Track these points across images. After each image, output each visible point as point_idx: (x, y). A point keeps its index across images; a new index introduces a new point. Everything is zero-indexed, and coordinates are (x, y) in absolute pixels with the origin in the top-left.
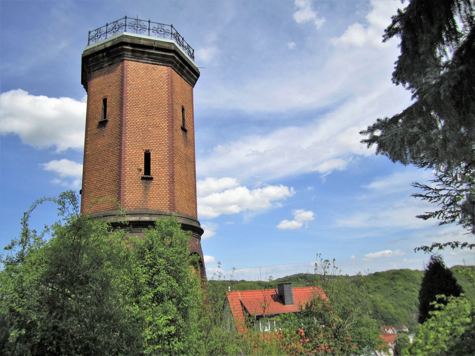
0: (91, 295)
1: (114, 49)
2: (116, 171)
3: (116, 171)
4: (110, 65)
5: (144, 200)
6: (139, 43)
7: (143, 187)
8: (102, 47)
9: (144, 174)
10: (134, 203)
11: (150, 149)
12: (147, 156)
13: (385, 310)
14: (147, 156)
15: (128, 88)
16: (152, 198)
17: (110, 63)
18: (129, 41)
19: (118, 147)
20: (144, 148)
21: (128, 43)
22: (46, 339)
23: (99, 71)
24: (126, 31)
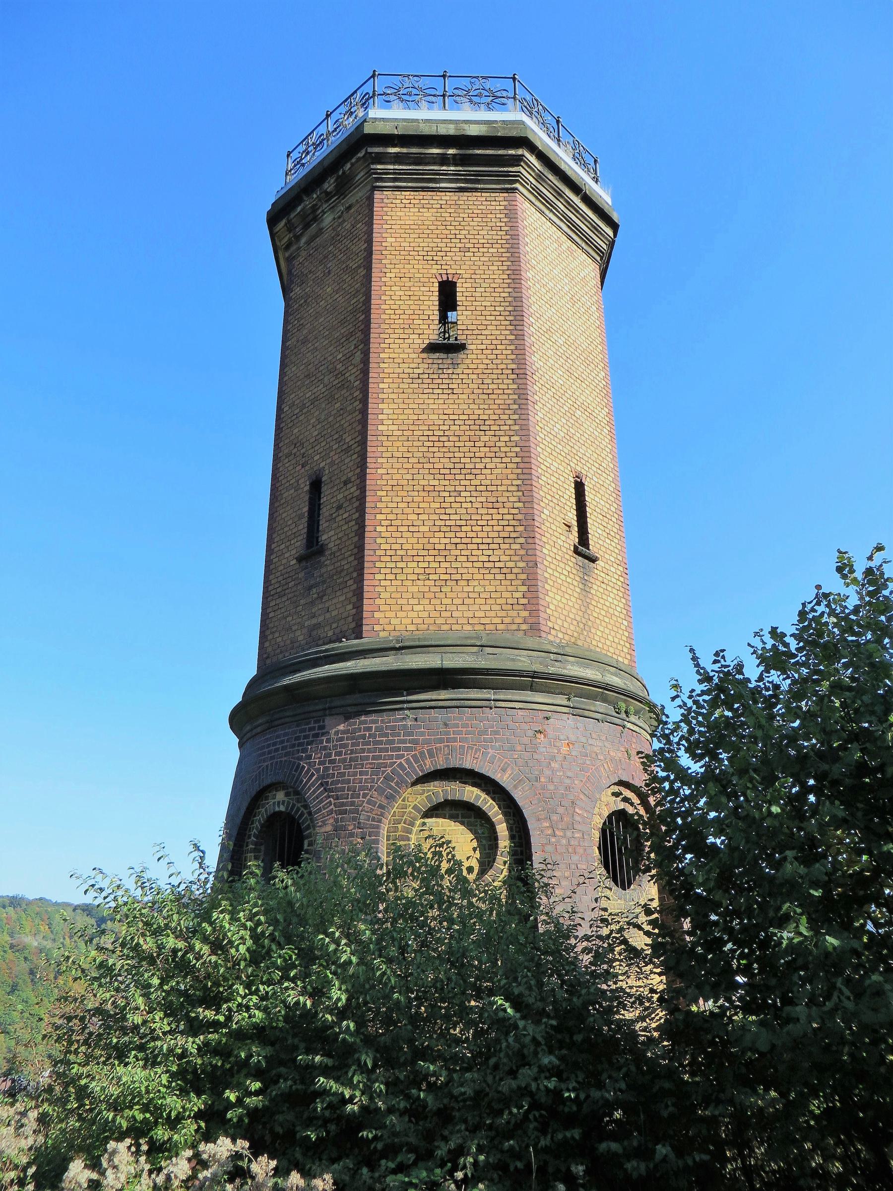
12: (579, 488)
14: (579, 488)
16: (598, 621)
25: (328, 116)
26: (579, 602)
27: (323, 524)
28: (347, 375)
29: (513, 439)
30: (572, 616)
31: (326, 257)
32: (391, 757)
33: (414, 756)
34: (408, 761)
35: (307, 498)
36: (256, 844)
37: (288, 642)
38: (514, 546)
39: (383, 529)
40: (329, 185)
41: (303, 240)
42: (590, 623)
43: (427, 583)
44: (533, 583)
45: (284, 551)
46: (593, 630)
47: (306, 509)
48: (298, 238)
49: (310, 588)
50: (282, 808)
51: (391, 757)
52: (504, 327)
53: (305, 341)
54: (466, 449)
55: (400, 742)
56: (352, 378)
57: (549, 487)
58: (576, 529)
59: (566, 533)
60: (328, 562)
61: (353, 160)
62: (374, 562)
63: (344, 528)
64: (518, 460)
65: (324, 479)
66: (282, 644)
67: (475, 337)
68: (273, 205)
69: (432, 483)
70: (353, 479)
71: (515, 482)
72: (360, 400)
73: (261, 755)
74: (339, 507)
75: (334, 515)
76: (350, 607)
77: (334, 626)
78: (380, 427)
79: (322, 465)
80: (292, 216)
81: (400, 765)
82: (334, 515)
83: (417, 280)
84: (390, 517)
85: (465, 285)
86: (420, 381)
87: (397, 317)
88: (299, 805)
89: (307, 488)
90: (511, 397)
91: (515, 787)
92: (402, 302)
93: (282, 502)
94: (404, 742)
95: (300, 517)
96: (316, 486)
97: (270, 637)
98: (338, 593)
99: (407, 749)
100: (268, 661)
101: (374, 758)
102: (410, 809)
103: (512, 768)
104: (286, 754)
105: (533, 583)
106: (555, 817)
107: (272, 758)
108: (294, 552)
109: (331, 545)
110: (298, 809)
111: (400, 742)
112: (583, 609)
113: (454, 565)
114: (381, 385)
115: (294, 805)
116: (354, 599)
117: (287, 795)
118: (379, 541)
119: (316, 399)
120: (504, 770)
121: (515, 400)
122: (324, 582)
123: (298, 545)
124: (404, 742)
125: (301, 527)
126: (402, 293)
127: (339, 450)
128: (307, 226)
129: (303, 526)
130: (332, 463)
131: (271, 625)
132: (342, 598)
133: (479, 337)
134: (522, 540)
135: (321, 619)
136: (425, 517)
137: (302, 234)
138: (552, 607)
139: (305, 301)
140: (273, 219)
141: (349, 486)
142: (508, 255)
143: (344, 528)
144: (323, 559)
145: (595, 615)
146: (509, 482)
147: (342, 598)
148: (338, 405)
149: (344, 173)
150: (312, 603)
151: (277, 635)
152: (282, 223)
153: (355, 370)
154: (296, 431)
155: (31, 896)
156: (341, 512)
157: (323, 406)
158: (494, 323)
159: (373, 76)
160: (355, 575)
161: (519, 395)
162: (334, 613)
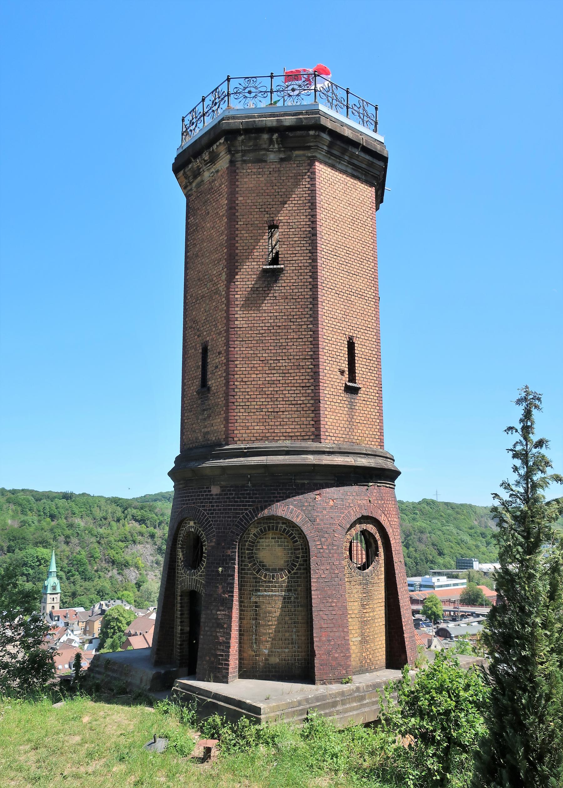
0: (499, 632)
1: (299, 133)
2: (308, 370)
3: (308, 370)
4: (282, 160)
5: (349, 426)
6: (342, 133)
7: (347, 403)
8: (271, 121)
9: (347, 379)
10: (337, 432)
11: (355, 335)
12: (351, 346)
13: (12, 496)
14: (351, 346)
15: (321, 215)
16: (359, 425)
17: (282, 156)
18: (329, 125)
19: (311, 326)
20: (347, 333)
21: (359, 144)
22: (223, 628)
23: (257, 166)
24: (376, 132)
25: (203, 100)
26: (347, 416)
27: (209, 376)
28: (219, 286)
29: (309, 326)
30: (341, 425)
31: (206, 202)
32: (242, 509)
33: (253, 509)
34: (250, 512)
35: (201, 357)
36: (182, 545)
37: (194, 439)
38: (308, 391)
39: (238, 383)
40: (206, 156)
41: (194, 184)
42: (353, 427)
43: (262, 413)
44: (318, 412)
45: (191, 385)
46: (355, 431)
47: (200, 363)
48: (191, 183)
49: (204, 410)
50: (193, 530)
51: (242, 509)
52: (305, 255)
53: (197, 256)
54: (283, 334)
55: (247, 502)
56: (221, 289)
57: (330, 352)
58: (347, 373)
59: (341, 377)
60: (211, 398)
61: (218, 144)
62: (233, 403)
63: (219, 380)
64: (311, 339)
65: (209, 348)
66: (191, 439)
67: (288, 262)
68: (176, 159)
69: (264, 355)
70: (223, 352)
71: (309, 353)
72: (225, 310)
73: (183, 500)
74: (216, 367)
75: (214, 371)
76: (222, 426)
77: (216, 435)
78: (236, 323)
79: (208, 339)
80: (187, 170)
81: (246, 514)
82: (214, 371)
83: (256, 225)
84: (242, 376)
85: (284, 227)
86: (258, 292)
87: (245, 251)
88: (200, 529)
89: (201, 351)
90: (309, 300)
91: (303, 525)
92: (247, 241)
93: (189, 355)
94: (248, 502)
95: (198, 367)
96: (205, 351)
97: (186, 433)
98: (217, 417)
99: (249, 506)
100: (185, 447)
101: (234, 509)
102: (252, 535)
103: (302, 515)
104: (194, 503)
105: (318, 412)
106: (323, 540)
107: (187, 504)
108: (195, 387)
109: (213, 388)
110: (200, 531)
111: (247, 502)
112: (349, 420)
113: (276, 403)
114: (236, 296)
115: (198, 529)
116: (224, 422)
117: (195, 523)
118: (236, 390)
119: (203, 296)
120: (297, 517)
121: (311, 302)
122: (210, 409)
123: (198, 382)
124: (248, 502)
125: (198, 373)
126: (247, 235)
127: (216, 333)
128: (195, 177)
129: (199, 372)
130: (212, 339)
131: (186, 427)
132: (219, 420)
133: (291, 262)
134: (312, 388)
135: (209, 429)
136: (260, 376)
137: (193, 182)
138: (329, 423)
139: (196, 228)
140: (177, 168)
141: (221, 355)
142: (309, 204)
143: (219, 380)
144: (209, 395)
145: (357, 421)
146: (306, 353)
147: (219, 420)
148: (214, 304)
149: (213, 150)
150: (205, 419)
151: (189, 433)
152: (182, 172)
153: (222, 284)
154: (194, 313)
155: (77, 492)
156: (217, 370)
157: (207, 302)
158: (300, 252)
159: (228, 79)
160: (224, 408)
161: (313, 299)
162: (215, 428)
